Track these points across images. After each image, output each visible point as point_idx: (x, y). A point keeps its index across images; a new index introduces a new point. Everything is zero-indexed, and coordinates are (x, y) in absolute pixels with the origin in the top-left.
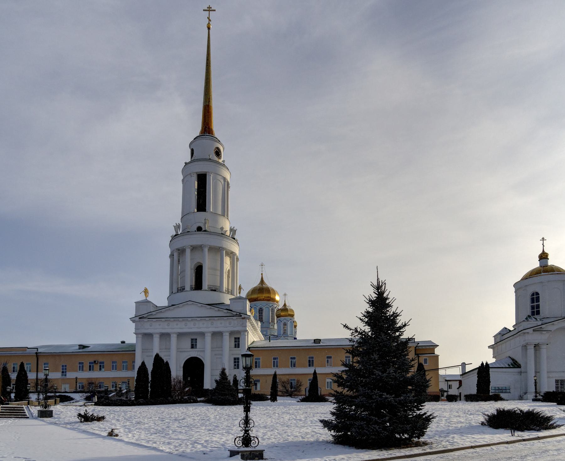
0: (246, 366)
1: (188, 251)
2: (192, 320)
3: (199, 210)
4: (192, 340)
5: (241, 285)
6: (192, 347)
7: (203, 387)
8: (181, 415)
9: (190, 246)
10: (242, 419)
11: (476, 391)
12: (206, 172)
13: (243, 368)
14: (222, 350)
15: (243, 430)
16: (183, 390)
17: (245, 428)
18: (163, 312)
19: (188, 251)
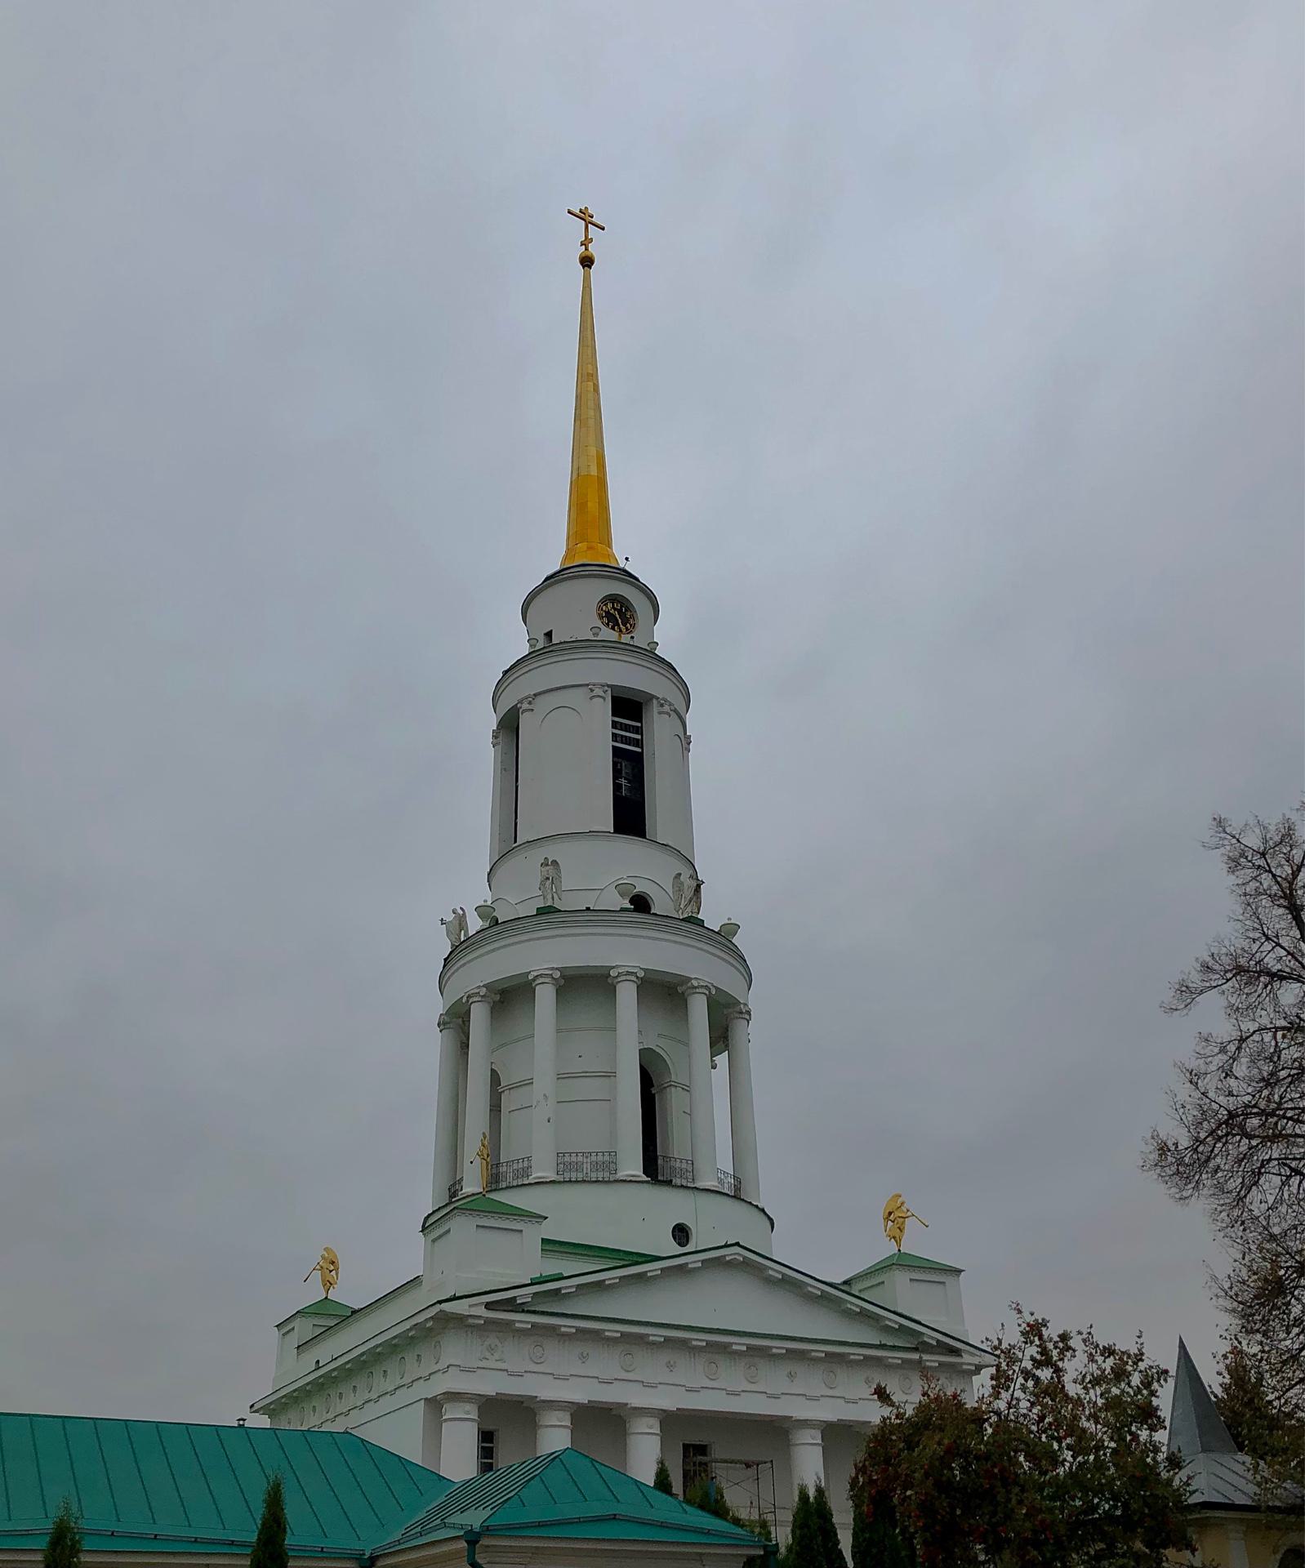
1: (545, 995)
9: (483, 991)
19: (545, 995)
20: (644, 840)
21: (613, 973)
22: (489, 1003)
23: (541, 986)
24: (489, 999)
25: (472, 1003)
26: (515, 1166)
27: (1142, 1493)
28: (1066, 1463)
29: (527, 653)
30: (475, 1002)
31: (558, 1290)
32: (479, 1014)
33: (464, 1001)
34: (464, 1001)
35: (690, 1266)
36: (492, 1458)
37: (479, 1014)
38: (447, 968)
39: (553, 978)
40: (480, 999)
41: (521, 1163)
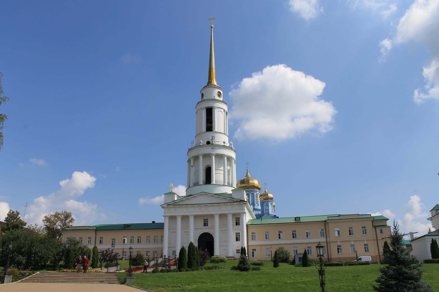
0: (320, 254)
1: (201, 158)
12: (212, 107)
18: (190, 199)
19: (201, 158)
37: (192, 161)
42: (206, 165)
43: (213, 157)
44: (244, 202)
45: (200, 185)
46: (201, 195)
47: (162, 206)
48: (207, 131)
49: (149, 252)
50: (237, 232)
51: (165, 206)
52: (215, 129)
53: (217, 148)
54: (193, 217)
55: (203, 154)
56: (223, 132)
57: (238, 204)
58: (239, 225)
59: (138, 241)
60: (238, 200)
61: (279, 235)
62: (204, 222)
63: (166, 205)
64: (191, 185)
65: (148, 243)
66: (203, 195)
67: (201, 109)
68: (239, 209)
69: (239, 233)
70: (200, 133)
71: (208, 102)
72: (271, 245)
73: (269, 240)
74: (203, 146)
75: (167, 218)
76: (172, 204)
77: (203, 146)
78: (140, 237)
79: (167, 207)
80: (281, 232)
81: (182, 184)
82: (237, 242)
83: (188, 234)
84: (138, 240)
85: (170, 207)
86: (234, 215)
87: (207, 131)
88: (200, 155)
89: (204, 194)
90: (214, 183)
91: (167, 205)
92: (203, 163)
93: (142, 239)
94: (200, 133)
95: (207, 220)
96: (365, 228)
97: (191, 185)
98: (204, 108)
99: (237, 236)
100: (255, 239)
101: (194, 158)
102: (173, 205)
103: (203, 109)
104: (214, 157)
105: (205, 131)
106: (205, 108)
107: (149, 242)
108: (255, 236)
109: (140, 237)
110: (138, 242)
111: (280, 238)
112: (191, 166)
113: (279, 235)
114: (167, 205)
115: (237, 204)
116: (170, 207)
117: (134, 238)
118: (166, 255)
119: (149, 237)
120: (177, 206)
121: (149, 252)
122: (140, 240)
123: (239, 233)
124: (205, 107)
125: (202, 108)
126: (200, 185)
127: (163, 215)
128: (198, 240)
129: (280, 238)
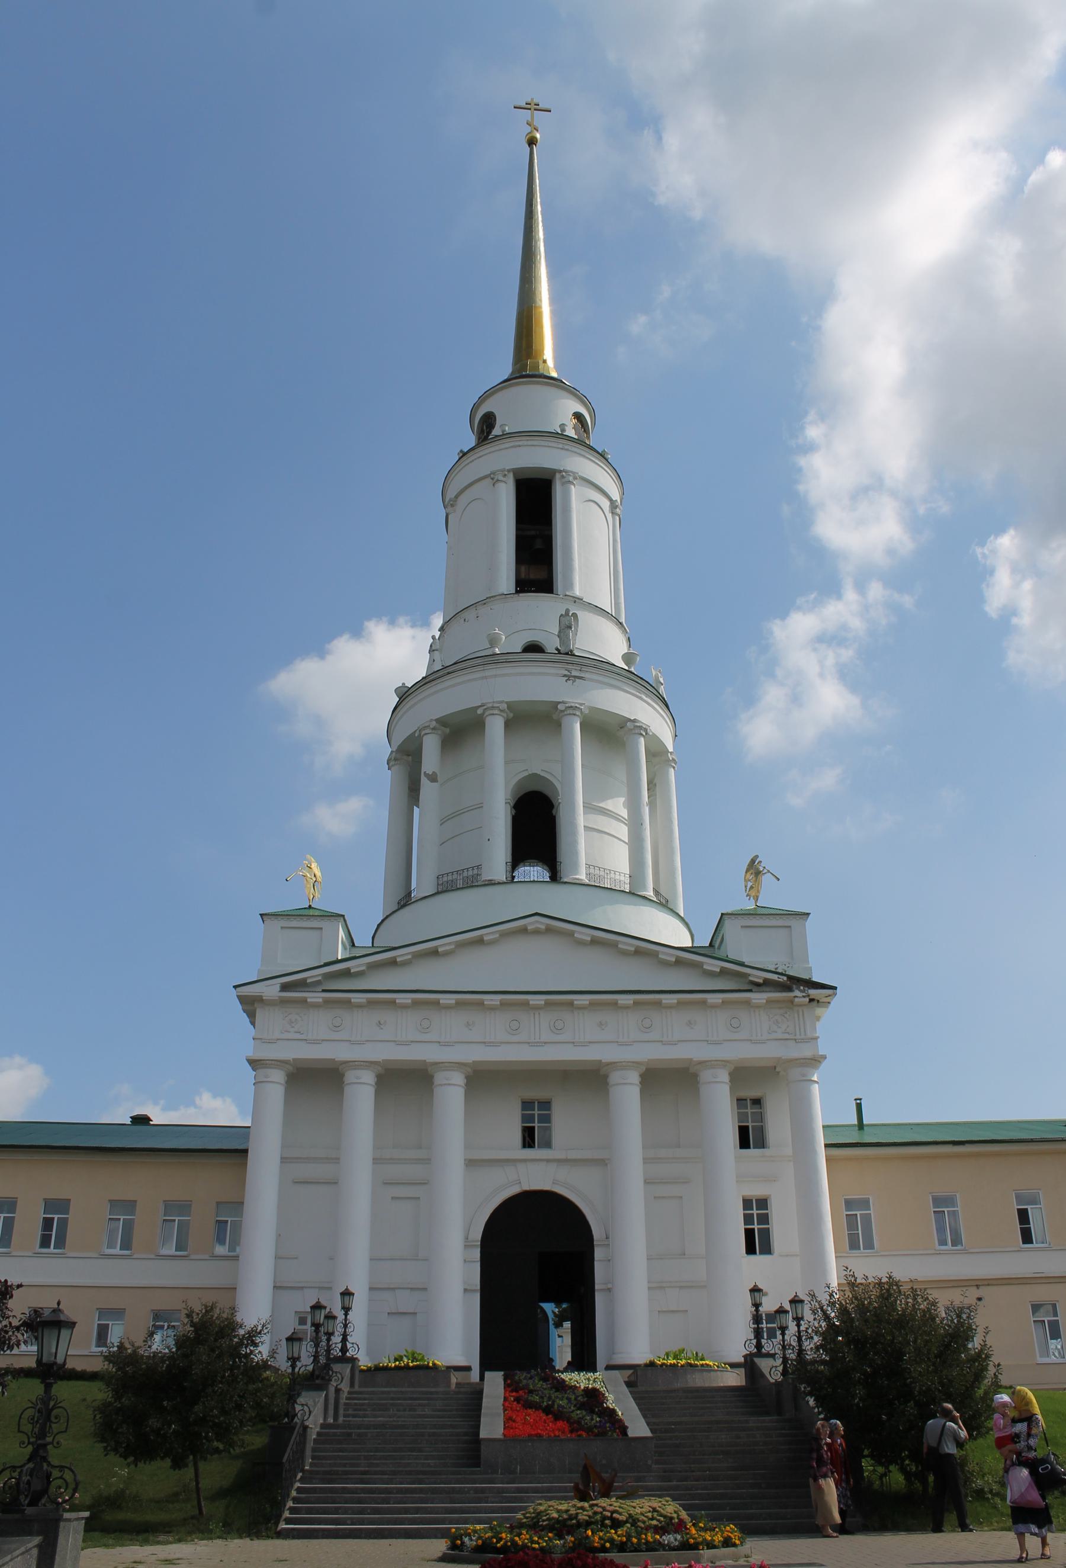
0: (797, 1316)
1: (496, 726)
2: (636, 1003)
3: (524, 585)
4: (527, 1105)
5: (757, 856)
6: (529, 1139)
7: (503, 1375)
8: (96, 1413)
9: (434, 724)
10: (30, 1405)
11: (501, 1430)
12: (554, 472)
13: (793, 1319)
14: (427, 1161)
15: (29, 1443)
16: (567, 1397)
17: (38, 1438)
18: (447, 954)
19: (496, 726)
20: (552, 595)
21: (561, 707)
22: (503, 717)
23: (490, 717)
24: (440, 732)
25: (487, 716)
26: (465, 874)
27: (858, 1392)
28: (851, 1339)
29: (458, 459)
30: (426, 734)
31: (305, 979)
32: (431, 746)
33: (416, 735)
34: (416, 735)
35: (308, 981)
36: (767, 1210)
37: (431, 746)
38: (394, 714)
39: (500, 710)
40: (499, 713)
41: (451, 876)
42: (521, 772)
43: (572, 729)
44: (813, 992)
45: (491, 883)
46: (524, 931)
47: (245, 990)
48: (517, 592)
49: (118, 1313)
50: (756, 1191)
51: (271, 991)
52: (570, 585)
53: (595, 677)
54: (458, 1079)
55: (511, 706)
56: (607, 605)
57: (777, 1001)
58: (762, 1144)
59: (43, 1236)
60: (775, 977)
61: (1023, 1215)
62: (525, 1118)
63: (278, 988)
64: (421, 883)
65: (117, 1251)
66: (537, 932)
67: (488, 480)
68: (779, 1035)
69: (763, 1203)
70: (483, 602)
71: (530, 443)
72: (978, 1284)
73: (966, 1252)
74: (504, 659)
75: (278, 1076)
76: (318, 983)
77: (504, 659)
78: (60, 1205)
79: (283, 1002)
80: (1034, 1201)
81: (639, 738)
82: (752, 1257)
83: (241, 1202)
84: (48, 1223)
85: (304, 1002)
86: (740, 1074)
87: (517, 592)
88: (493, 708)
89: (543, 927)
90: (582, 876)
91: (285, 987)
92: (507, 762)
93: (73, 1217)
94: (483, 602)
95: (546, 1105)
96: (133, 1213)
97: (421, 883)
98: (509, 471)
99: (748, 1219)
100: (869, 1245)
101: (448, 730)
102: (324, 991)
103: (501, 478)
104: (577, 727)
105: (512, 588)
106: (511, 476)
107: (126, 1245)
108: (867, 1219)
109: (60, 1205)
110: (45, 1242)
111: (1027, 1237)
112: (426, 775)
113: (1023, 1215)
114: (285, 987)
115: (769, 1002)
116: (304, 1002)
117: (133, 1213)
118: (69, 1312)
119: (130, 1206)
120: (356, 998)
121: (118, 1313)
122: (63, 1224)
123: (763, 1203)
124: (515, 472)
125: (493, 473)
126: (491, 883)
127: (250, 1054)
128: (482, 1238)
129: (1027, 1237)
